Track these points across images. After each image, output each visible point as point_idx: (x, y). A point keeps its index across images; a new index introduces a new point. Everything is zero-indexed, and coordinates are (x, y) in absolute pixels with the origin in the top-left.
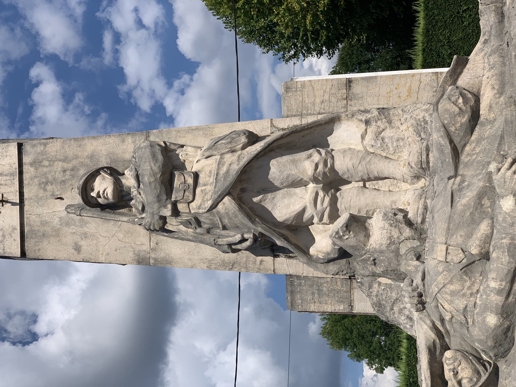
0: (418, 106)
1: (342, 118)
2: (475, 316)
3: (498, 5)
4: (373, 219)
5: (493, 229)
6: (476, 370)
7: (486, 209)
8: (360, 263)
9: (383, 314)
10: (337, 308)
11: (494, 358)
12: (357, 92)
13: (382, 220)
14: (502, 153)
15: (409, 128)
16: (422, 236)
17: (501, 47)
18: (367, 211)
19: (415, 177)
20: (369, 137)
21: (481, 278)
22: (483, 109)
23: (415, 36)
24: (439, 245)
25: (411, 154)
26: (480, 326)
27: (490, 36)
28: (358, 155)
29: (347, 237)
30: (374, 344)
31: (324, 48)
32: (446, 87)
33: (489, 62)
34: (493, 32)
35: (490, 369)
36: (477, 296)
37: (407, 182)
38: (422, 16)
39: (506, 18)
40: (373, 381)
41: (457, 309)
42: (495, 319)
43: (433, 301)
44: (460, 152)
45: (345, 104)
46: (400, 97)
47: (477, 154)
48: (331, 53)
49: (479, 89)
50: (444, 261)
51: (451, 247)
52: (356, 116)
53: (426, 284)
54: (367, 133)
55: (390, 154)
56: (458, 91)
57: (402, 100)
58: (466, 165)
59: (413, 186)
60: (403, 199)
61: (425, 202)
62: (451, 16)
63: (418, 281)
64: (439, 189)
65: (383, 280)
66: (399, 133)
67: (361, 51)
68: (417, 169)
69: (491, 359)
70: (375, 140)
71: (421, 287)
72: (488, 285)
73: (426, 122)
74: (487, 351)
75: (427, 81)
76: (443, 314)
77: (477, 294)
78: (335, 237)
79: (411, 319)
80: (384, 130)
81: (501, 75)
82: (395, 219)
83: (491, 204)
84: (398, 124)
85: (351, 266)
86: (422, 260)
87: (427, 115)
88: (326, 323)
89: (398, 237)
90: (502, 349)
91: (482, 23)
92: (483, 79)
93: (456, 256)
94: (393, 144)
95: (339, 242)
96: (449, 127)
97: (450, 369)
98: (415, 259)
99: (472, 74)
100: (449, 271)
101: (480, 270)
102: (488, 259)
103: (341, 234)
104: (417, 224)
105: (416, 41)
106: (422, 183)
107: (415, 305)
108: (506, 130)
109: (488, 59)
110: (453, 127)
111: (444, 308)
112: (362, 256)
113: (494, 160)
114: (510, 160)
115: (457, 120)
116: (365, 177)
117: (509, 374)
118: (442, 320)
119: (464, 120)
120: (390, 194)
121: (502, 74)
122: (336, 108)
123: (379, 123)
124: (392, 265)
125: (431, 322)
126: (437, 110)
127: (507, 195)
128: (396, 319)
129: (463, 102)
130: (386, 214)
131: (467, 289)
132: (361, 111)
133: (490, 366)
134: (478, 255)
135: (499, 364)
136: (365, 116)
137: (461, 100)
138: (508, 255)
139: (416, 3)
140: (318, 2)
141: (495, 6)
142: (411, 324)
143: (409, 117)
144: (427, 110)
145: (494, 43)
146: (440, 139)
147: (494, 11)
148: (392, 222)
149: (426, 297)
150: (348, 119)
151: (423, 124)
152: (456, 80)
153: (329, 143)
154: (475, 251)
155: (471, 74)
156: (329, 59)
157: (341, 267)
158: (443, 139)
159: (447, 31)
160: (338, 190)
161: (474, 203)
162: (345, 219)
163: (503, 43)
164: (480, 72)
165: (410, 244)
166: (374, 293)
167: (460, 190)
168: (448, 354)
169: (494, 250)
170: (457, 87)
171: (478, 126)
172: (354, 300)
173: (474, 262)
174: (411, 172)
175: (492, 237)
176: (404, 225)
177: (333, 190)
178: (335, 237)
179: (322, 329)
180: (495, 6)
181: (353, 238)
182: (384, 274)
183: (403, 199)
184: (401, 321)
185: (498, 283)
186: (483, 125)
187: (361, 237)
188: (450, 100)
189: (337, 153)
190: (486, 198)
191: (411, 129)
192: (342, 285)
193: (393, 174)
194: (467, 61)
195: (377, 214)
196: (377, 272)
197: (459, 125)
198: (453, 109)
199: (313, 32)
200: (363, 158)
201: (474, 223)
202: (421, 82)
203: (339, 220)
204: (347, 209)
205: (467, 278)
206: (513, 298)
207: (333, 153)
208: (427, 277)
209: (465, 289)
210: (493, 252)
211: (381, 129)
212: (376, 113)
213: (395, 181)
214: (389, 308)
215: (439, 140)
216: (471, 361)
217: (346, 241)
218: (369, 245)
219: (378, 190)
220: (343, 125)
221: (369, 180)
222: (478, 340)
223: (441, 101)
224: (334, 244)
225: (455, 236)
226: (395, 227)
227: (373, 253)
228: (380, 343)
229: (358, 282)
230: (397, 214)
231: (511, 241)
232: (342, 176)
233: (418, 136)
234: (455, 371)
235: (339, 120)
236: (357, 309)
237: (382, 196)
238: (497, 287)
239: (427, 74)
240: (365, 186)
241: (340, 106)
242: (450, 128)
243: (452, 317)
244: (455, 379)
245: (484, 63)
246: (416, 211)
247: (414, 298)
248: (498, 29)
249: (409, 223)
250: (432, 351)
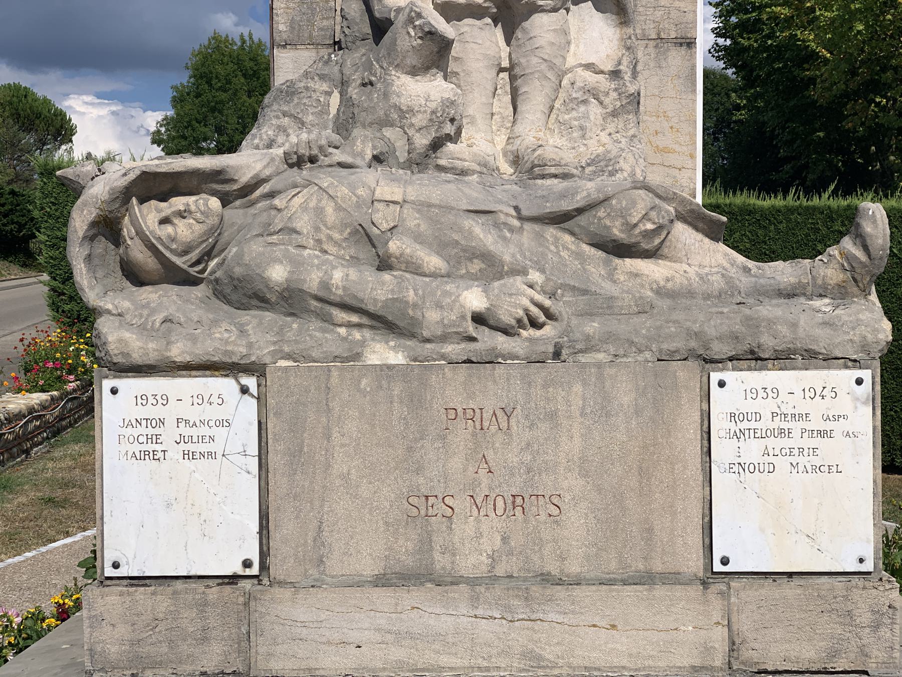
0: (641, 161)
1: (625, 29)
2: (282, 247)
3: (810, 288)
4: (444, 82)
5: (430, 276)
6: (191, 248)
7: (464, 267)
8: (364, 59)
9: (275, 99)
10: (280, 18)
11: (212, 278)
12: (670, 59)
13: (442, 98)
14: (559, 291)
15: (604, 145)
16: (415, 166)
17: (736, 293)
18: (457, 74)
19: (518, 157)
20: (591, 78)
21: (348, 258)
22: (633, 263)
23: (742, 191)
24: (402, 190)
25: (557, 149)
26: (267, 255)
27: (755, 276)
28: (557, 57)
29: (413, 34)
30: (203, 129)
31: (728, 42)
32: (673, 203)
33: (712, 275)
34: (762, 281)
35: (193, 271)
36: (316, 250)
37: (507, 144)
38: (777, 203)
39: (786, 301)
40: (138, 128)
41: (293, 217)
42: (280, 279)
43: (305, 180)
44: (562, 225)
45: (650, 35)
46: (657, 134)
47: (558, 253)
48: (720, 53)
49: (667, 257)
50: (375, 198)
51: (398, 209)
52: (627, 54)
53: (333, 169)
54: (596, 74)
55: (558, 115)
56: (666, 222)
57: (651, 138)
58: (540, 236)
59: (501, 154)
60: (478, 136)
61: (474, 172)
62: (774, 252)
63: (339, 156)
64: (498, 192)
65: (335, 99)
66: (594, 129)
67: (717, 110)
68: (531, 159)
69: (211, 274)
70: (584, 89)
71: (327, 161)
72: (337, 267)
73: (612, 174)
74: (225, 266)
75: (682, 181)
76: (282, 196)
77: (320, 251)
78: (412, 10)
79: (269, 146)
80: (601, 103)
81: (689, 292)
82: (445, 120)
83: (473, 274)
84: (611, 128)
85: (358, 43)
86: (373, 165)
87: (625, 174)
88: (234, 43)
89: (412, 125)
90: (228, 291)
91: (779, 264)
92: (684, 265)
93: (383, 218)
94: (575, 119)
95: (402, 18)
96: (605, 208)
97: (188, 205)
98: (375, 153)
99: (693, 247)
100: (358, 206)
101: (361, 256)
102: (379, 269)
103: (417, 23)
104: (435, 157)
105: (734, 193)
106: (507, 169)
107: (295, 150)
108: (598, 298)
109: (718, 273)
110: (605, 214)
111: (294, 196)
112: (378, 63)
113: (548, 279)
114: (547, 303)
115: (617, 221)
116: (517, 71)
117: (187, 301)
118: (271, 195)
119: (616, 232)
120: (487, 114)
121: (690, 294)
122: (643, 18)
123: (614, 95)
124: (364, 114)
125: (267, 176)
126: (636, 188)
127: (488, 299)
128: (268, 121)
129: (646, 231)
130: (453, 103)
131: (328, 235)
132: (636, 64)
133: (197, 272)
134: (387, 252)
135: (202, 286)
136: (627, 70)
137: (650, 226)
138: (387, 299)
139: (801, 193)
140: (811, 30)
141: (808, 283)
142: (261, 146)
143: (623, 147)
144: (633, 174)
145: (745, 282)
146: (585, 194)
147: (800, 282)
148: (439, 115)
149: (311, 169)
150: (622, 39)
151: (610, 168)
152: (685, 220)
153: (580, 5)
154: (394, 246)
155: (694, 244)
156: (709, 50)
157: (357, 24)
158: (584, 197)
159: (748, 245)
160: (495, 22)
161: (474, 247)
162: (442, 30)
163: (744, 295)
164: (694, 261)
165: (401, 146)
166: (311, 84)
167: (497, 225)
168: (215, 203)
169: (395, 277)
170: (672, 221)
171: (604, 255)
172: (297, 51)
173: (374, 246)
174: (525, 150)
175: (417, 274)
176: (434, 135)
177: (495, 10)
178: (412, 10)
179: (224, 36)
180: (808, 283)
181: (409, 44)
182: (346, 101)
183: (477, 136)
184: (265, 130)
185: (340, 284)
186: (607, 263)
187: (412, 60)
188: (652, 208)
189: (563, 19)
190: (483, 266)
191: (601, 150)
192: (322, 29)
193: (523, 119)
194: (714, 237)
195: (453, 89)
196: (350, 89)
197: (608, 223)
198: (635, 213)
199: (758, 21)
200: (552, 66)
201: (441, 246)
202: (680, 170)
203: (442, 20)
204: (462, 36)
205: (346, 234)
206: (315, 307)
207: (563, 11)
208: (344, 172)
209: (328, 231)
210: (392, 275)
211: (603, 98)
212: (632, 89)
213: (510, 125)
214: (286, 108)
215: (583, 190)
216: (205, 241)
217: (404, 32)
218: (397, 74)
219: (494, 94)
220: (613, 30)
221: (513, 78)
222: (243, 251)
223: (651, 195)
224: (399, 10)
225: (417, 216)
226: (431, 120)
227: (384, 81)
228: (205, 140)
229: (330, 55)
230: (453, 124)
231: (411, 303)
232: (520, 27)
233: (588, 161)
234: (186, 214)
235: (621, 23)
236: (282, 55)
237: (484, 100)
238: (333, 281)
239: (693, 180)
240: (502, 70)
241: (647, 27)
242: (603, 210)
243: (279, 210)
244: (173, 213)
245: (711, 267)
246: (458, 156)
247: (308, 149)
248: (768, 288)
249: (436, 145)
250: (217, 176)
